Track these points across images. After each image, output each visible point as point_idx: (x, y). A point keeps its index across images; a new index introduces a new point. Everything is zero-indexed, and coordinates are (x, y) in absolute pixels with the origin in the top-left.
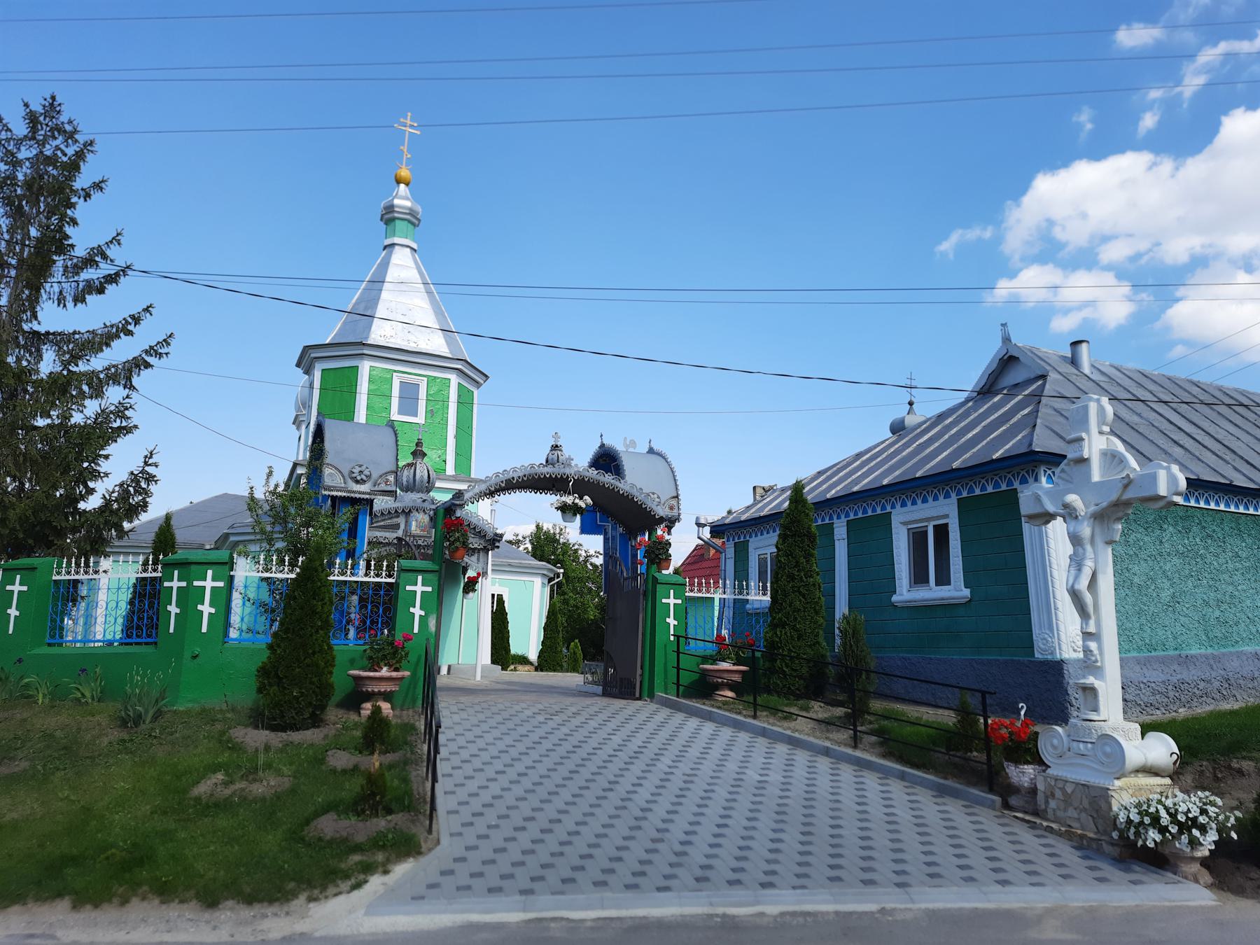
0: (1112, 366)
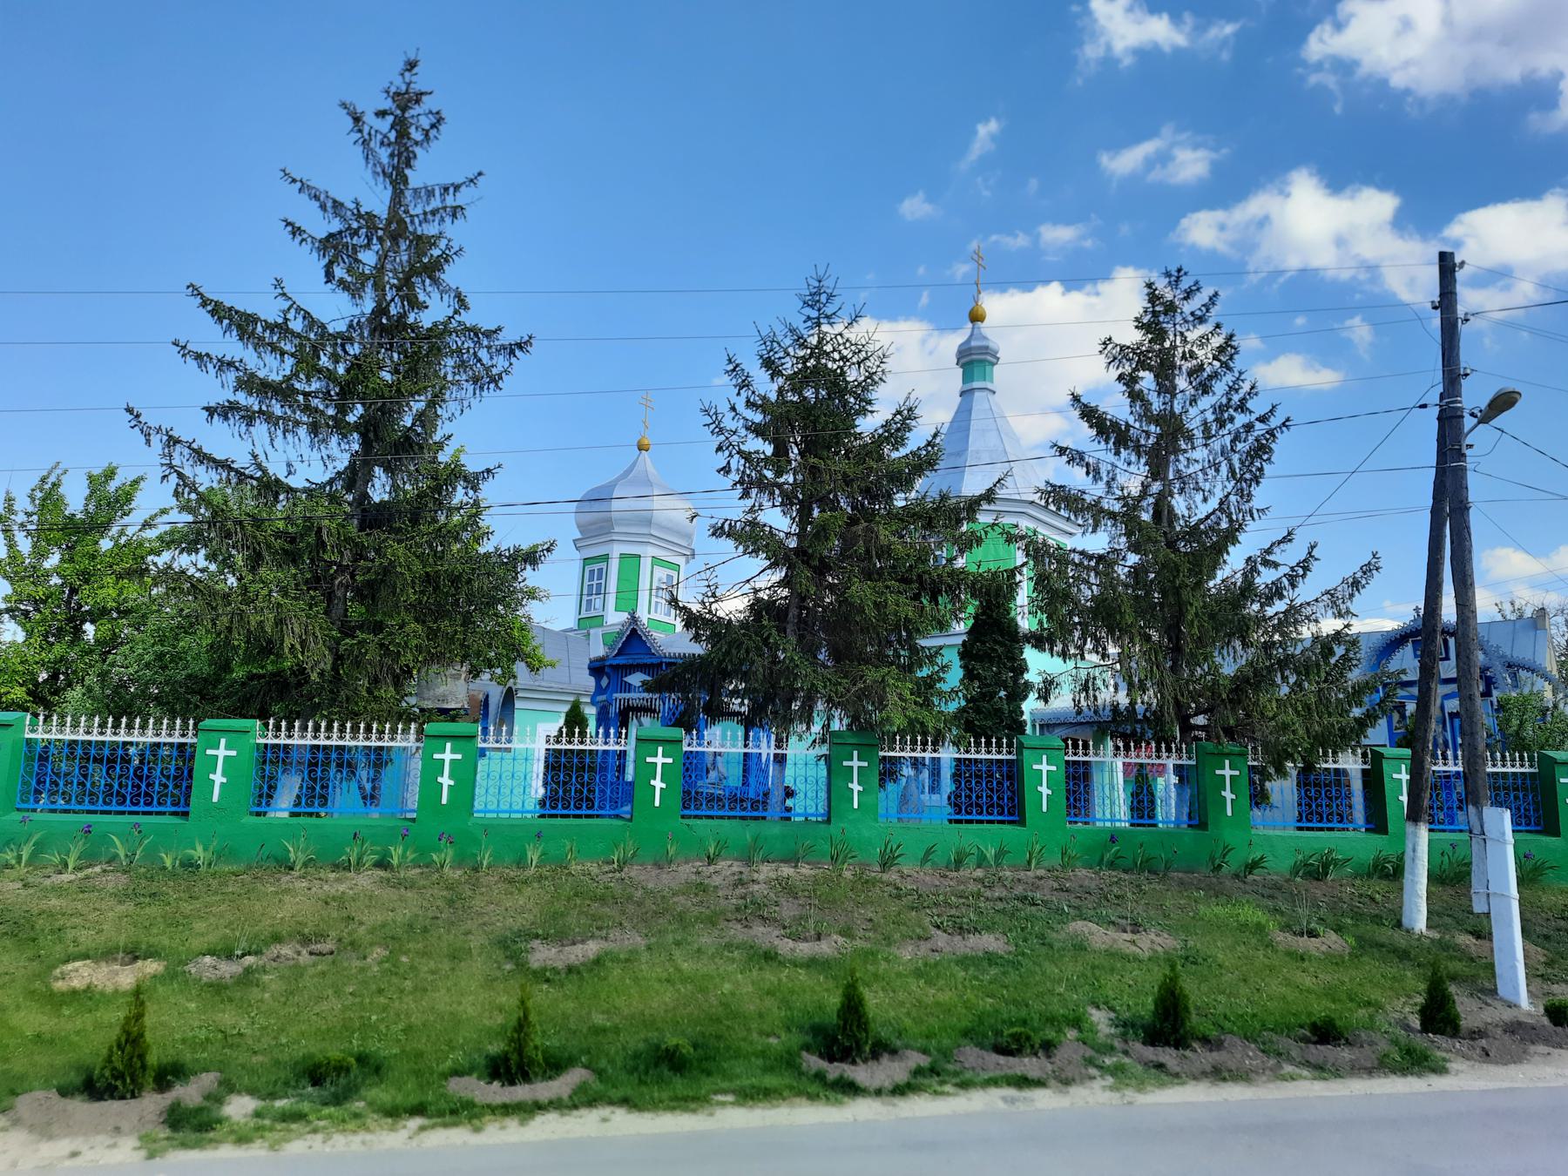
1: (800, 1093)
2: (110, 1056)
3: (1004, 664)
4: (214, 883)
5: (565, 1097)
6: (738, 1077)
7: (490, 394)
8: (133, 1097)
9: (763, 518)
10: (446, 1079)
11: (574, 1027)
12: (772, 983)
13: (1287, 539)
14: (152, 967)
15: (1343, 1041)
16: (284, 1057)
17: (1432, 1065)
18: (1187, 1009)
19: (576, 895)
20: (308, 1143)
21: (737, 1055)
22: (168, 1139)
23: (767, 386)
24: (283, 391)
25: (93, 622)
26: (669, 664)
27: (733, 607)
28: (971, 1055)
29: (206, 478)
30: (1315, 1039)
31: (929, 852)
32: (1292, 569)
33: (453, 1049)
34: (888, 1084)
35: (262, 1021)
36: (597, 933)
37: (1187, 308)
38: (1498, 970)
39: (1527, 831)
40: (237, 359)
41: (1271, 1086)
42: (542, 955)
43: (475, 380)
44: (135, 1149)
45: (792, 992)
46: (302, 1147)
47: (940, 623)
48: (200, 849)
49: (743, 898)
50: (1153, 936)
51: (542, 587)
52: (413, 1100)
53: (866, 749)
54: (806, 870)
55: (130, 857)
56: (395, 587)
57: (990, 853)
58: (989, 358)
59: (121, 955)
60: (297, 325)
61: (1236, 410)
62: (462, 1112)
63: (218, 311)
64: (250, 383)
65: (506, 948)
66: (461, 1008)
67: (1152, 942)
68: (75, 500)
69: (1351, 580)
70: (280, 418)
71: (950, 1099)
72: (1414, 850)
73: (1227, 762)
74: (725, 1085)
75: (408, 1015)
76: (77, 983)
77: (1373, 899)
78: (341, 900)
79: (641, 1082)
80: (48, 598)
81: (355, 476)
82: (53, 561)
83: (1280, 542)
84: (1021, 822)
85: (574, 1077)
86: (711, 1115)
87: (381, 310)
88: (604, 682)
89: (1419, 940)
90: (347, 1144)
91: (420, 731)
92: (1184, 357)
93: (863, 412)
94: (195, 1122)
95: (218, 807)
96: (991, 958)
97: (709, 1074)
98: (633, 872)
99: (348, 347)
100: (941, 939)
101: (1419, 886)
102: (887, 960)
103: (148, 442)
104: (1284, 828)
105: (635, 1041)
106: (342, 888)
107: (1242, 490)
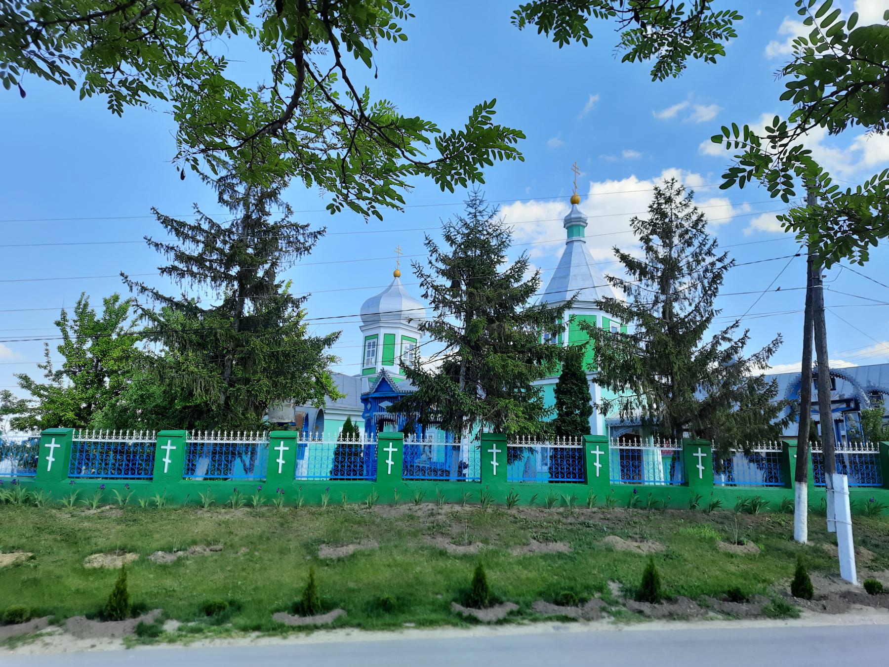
0: (77, 68)
1: (448, 623)
2: (110, 600)
3: (578, 396)
4: (165, 514)
5: (330, 623)
6: (418, 614)
7: (305, 257)
8: (121, 620)
9: (446, 320)
10: (272, 613)
11: (338, 589)
12: (442, 567)
13: (737, 325)
14: (130, 557)
15: (745, 600)
16: (195, 601)
17: (792, 614)
18: (658, 583)
19: (346, 521)
20: (202, 643)
21: (420, 603)
22: (136, 640)
23: (447, 250)
24: (199, 260)
25: (109, 376)
26: (402, 397)
27: (432, 367)
28: (541, 605)
29: (158, 307)
30: (730, 599)
31: (533, 498)
32: (736, 343)
33: (277, 599)
34: (494, 619)
35: (184, 584)
36: (355, 540)
37: (678, 199)
38: (841, 564)
39: (873, 487)
40: (175, 246)
41: (699, 623)
42: (326, 552)
43: (298, 249)
44: (121, 644)
45: (452, 571)
46: (199, 645)
47: (540, 374)
48: (158, 497)
49: (433, 523)
50: (650, 544)
51: (338, 356)
52: (255, 623)
53: (500, 443)
54: (467, 508)
55: (124, 501)
56: (255, 360)
57: (568, 499)
58: (581, 223)
59: (117, 551)
60: (205, 226)
61: (706, 255)
62: (279, 629)
63: (166, 222)
64: (182, 257)
65: (308, 548)
66: (283, 578)
67: (650, 547)
68: (100, 315)
69: (767, 349)
70: (198, 274)
71: (526, 627)
72: (799, 498)
73: (700, 449)
74: (411, 618)
75: (256, 582)
76: (96, 565)
77: (780, 524)
78: (227, 523)
79: (368, 616)
80: (85, 365)
81: (233, 304)
82: (89, 344)
83: (732, 327)
84: (585, 482)
85: (336, 613)
86: (401, 633)
87: (247, 217)
88: (369, 406)
89: (802, 547)
90: (221, 644)
91: (267, 435)
92: (677, 227)
93: (499, 262)
94: (150, 632)
95: (167, 475)
96: (560, 555)
97: (403, 612)
98: (376, 509)
99: (231, 236)
100: (535, 544)
101: (802, 517)
102: (504, 556)
103: (131, 290)
104: (751, 486)
105: (368, 596)
106: (228, 517)
107: (707, 300)
